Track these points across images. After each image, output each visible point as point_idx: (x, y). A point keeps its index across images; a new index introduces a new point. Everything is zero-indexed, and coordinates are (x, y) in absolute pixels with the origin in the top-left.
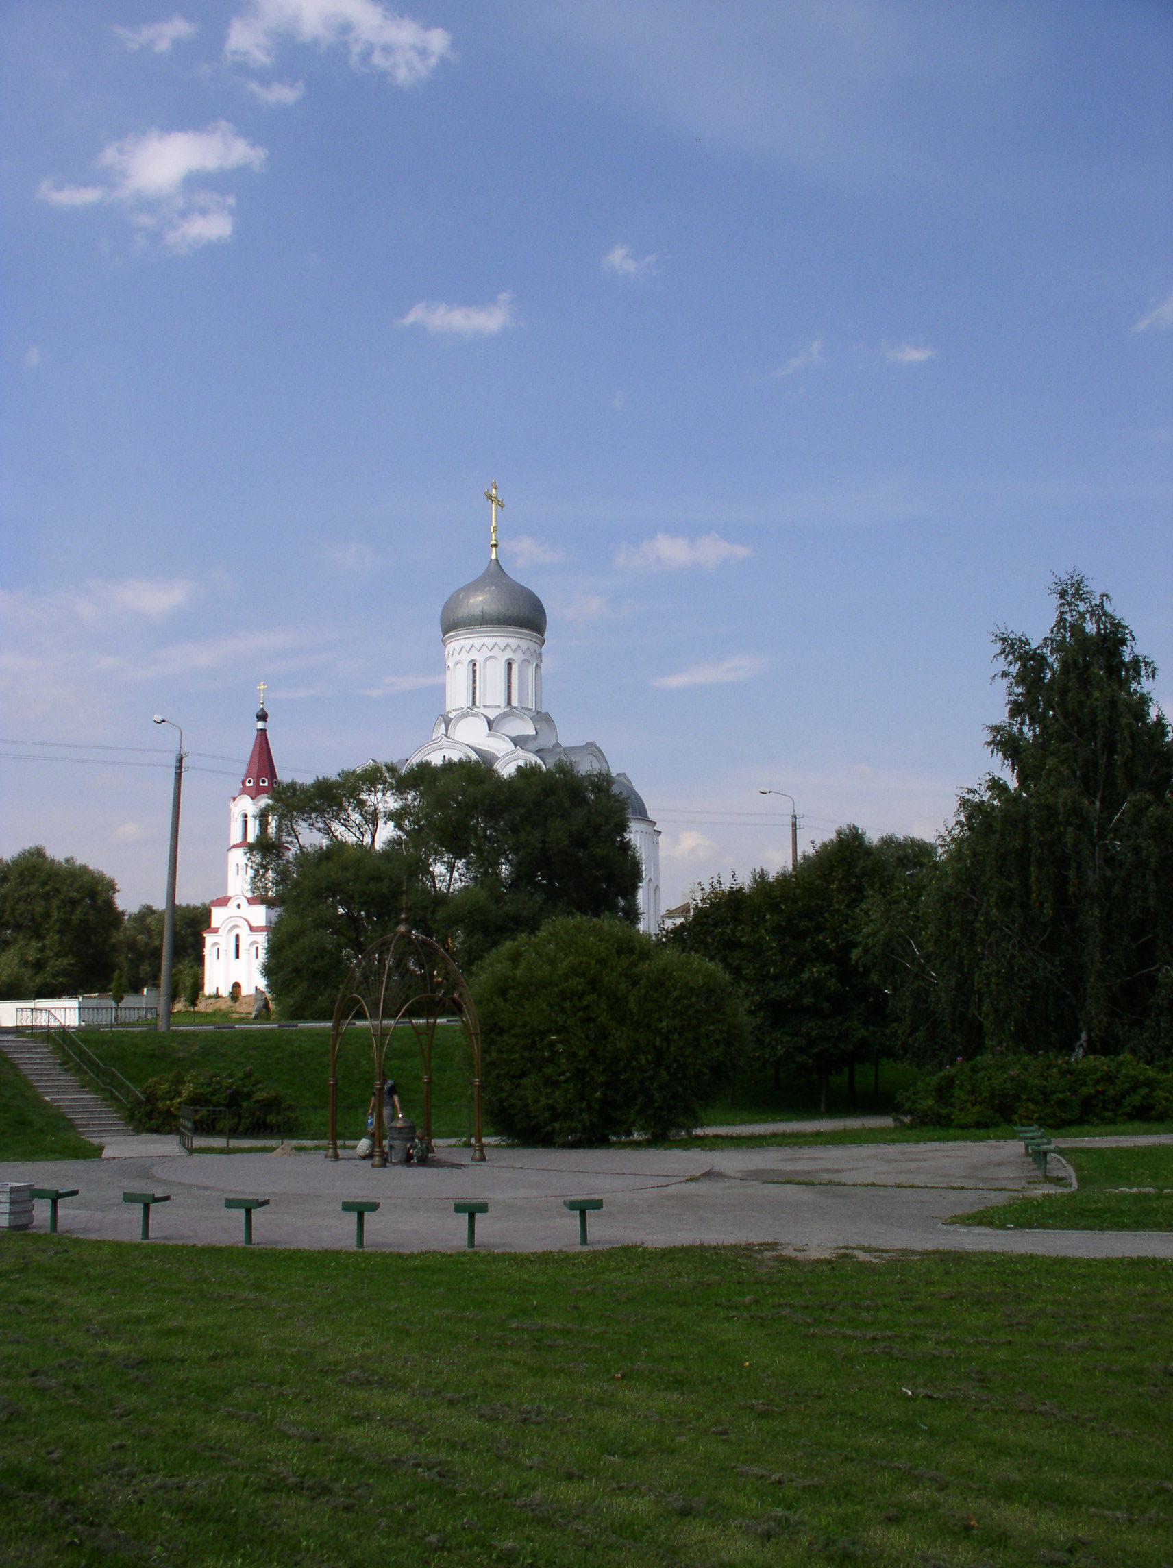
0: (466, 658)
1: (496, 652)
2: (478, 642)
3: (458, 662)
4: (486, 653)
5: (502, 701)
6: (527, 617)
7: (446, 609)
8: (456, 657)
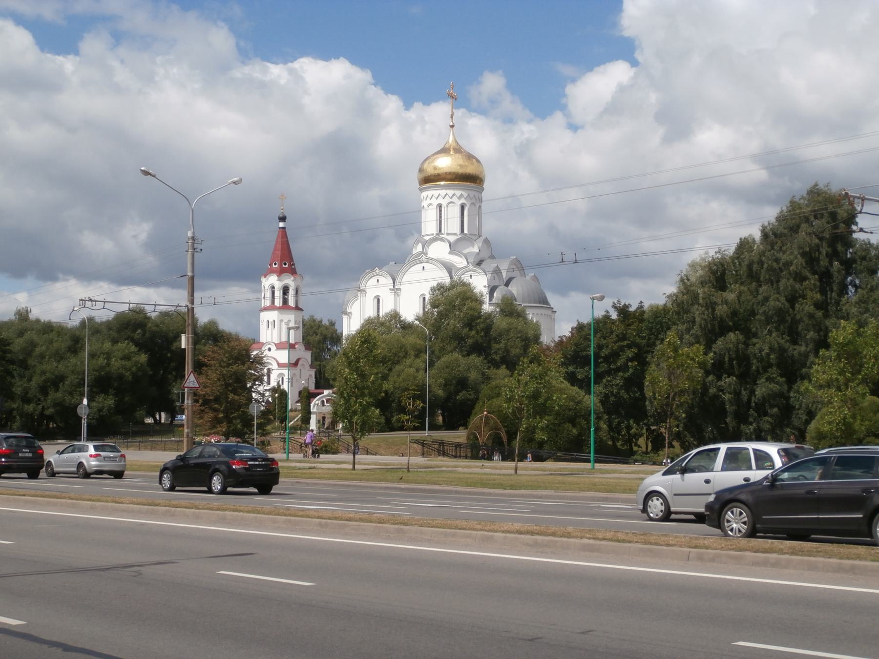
0: (435, 202)
1: (455, 199)
2: (443, 192)
3: (430, 205)
4: (448, 200)
5: (457, 230)
6: (470, 180)
7: (421, 170)
8: (429, 201)
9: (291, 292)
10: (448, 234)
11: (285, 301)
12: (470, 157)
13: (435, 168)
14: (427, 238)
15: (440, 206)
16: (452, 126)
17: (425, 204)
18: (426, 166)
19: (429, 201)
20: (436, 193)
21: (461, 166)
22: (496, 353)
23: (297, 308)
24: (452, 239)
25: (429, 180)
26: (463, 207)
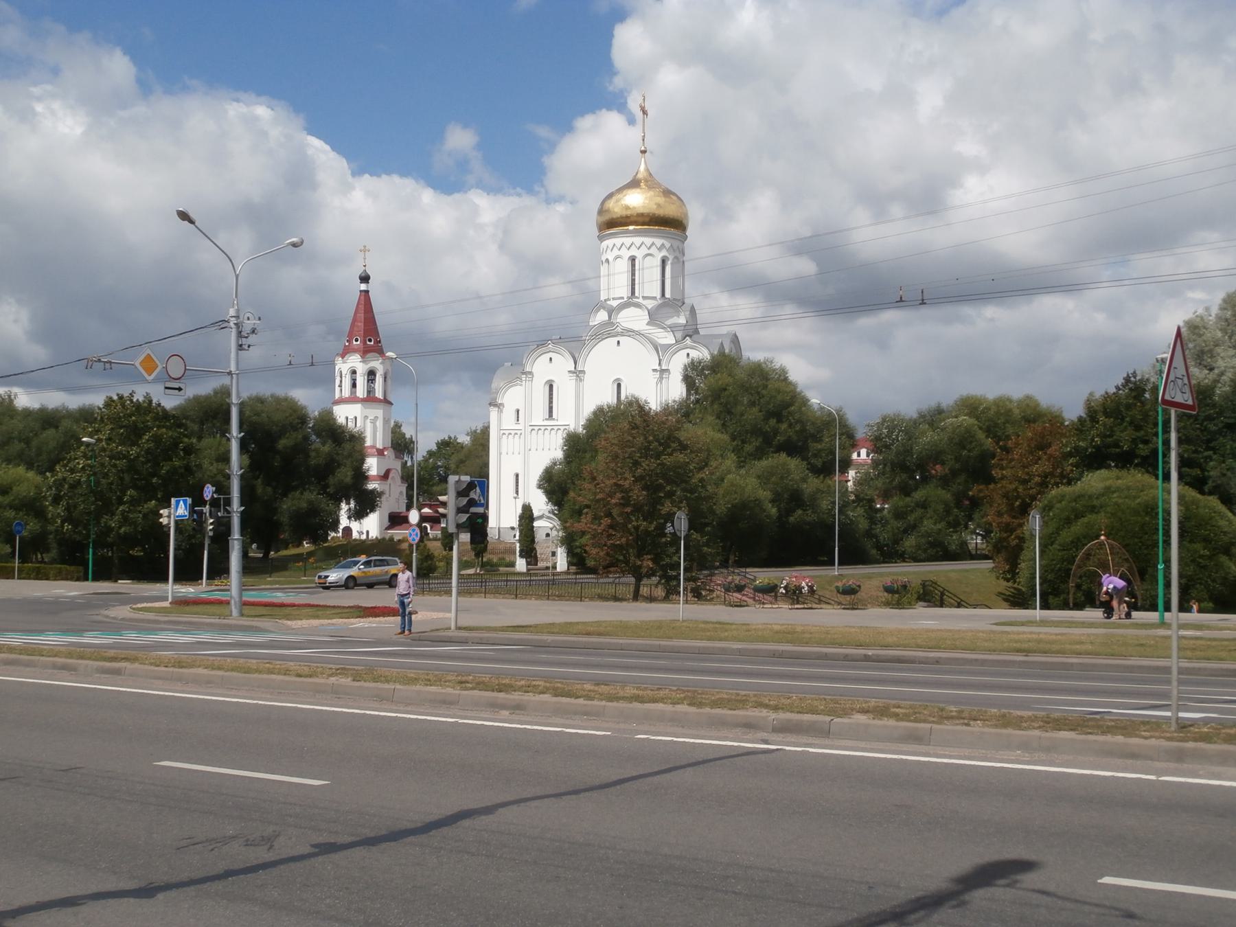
0: (626, 254)
1: (653, 250)
2: (638, 240)
4: (644, 251)
7: (601, 212)
8: (616, 252)
9: (379, 380)
10: (644, 298)
11: (370, 391)
12: (667, 193)
13: (627, 208)
14: (615, 303)
15: (633, 259)
16: (644, 152)
18: (611, 204)
19: (616, 252)
20: (628, 241)
21: (659, 205)
22: (815, 456)
23: (386, 401)
24: (650, 304)
25: (612, 224)
26: (664, 262)
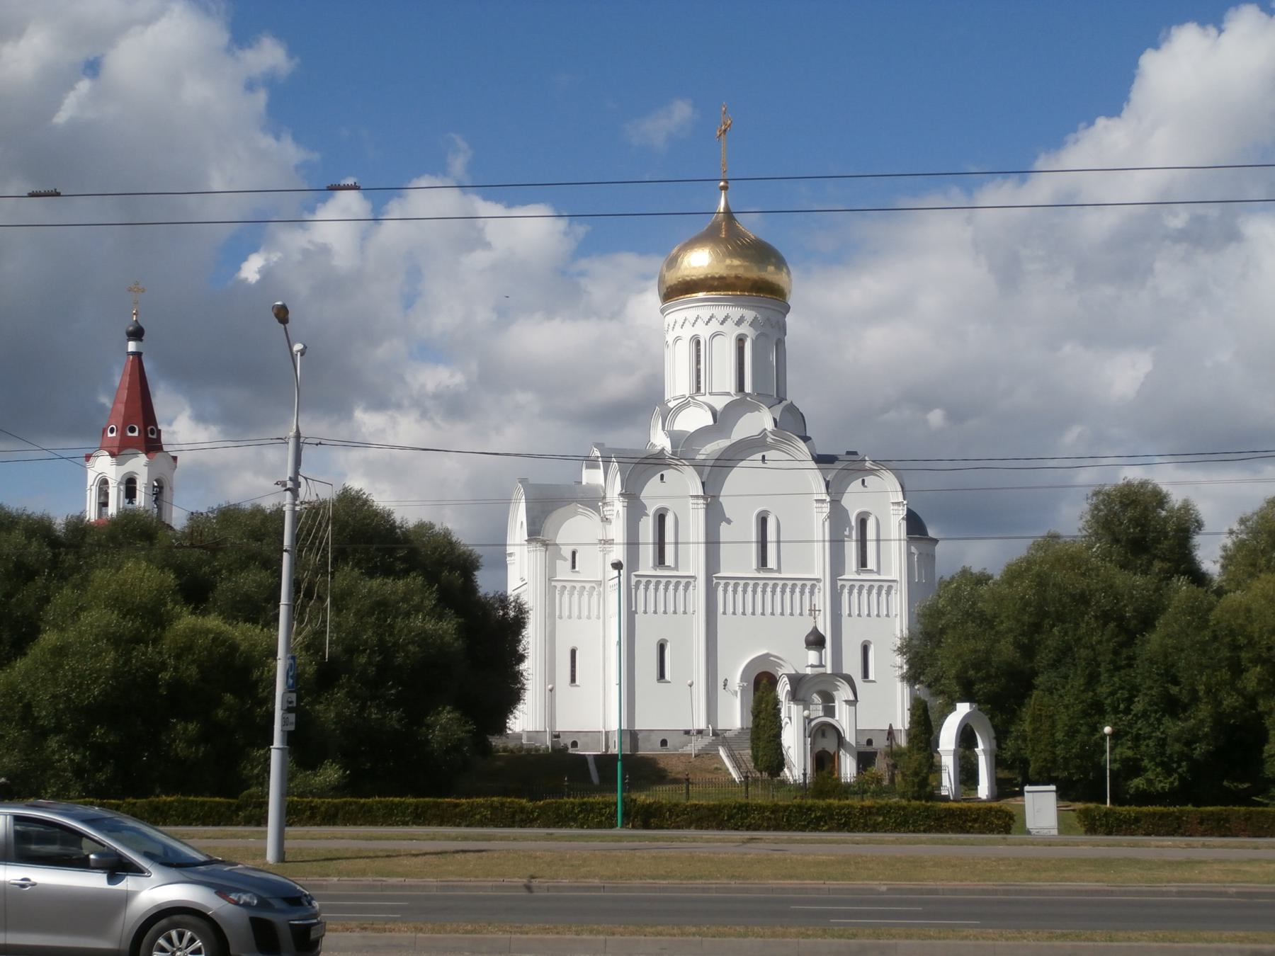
0: (688, 333)
2: (705, 312)
3: (677, 339)
4: (715, 326)
5: (731, 386)
8: (678, 331)
17: (670, 338)
20: (691, 314)
26: (741, 341)
